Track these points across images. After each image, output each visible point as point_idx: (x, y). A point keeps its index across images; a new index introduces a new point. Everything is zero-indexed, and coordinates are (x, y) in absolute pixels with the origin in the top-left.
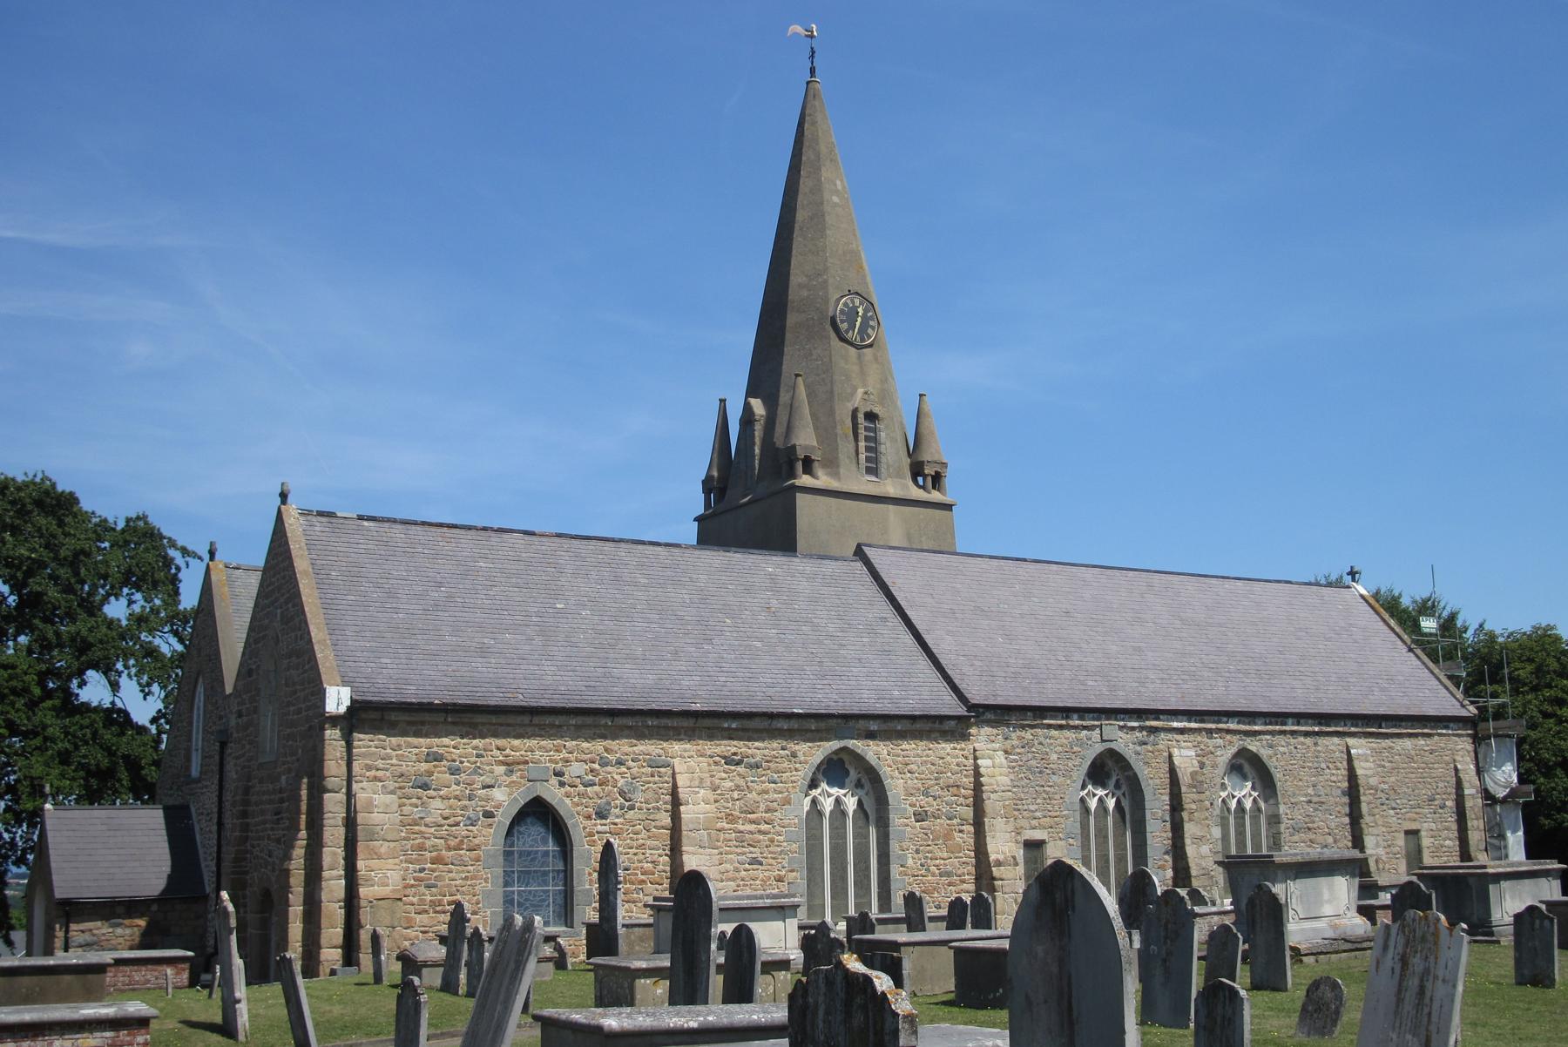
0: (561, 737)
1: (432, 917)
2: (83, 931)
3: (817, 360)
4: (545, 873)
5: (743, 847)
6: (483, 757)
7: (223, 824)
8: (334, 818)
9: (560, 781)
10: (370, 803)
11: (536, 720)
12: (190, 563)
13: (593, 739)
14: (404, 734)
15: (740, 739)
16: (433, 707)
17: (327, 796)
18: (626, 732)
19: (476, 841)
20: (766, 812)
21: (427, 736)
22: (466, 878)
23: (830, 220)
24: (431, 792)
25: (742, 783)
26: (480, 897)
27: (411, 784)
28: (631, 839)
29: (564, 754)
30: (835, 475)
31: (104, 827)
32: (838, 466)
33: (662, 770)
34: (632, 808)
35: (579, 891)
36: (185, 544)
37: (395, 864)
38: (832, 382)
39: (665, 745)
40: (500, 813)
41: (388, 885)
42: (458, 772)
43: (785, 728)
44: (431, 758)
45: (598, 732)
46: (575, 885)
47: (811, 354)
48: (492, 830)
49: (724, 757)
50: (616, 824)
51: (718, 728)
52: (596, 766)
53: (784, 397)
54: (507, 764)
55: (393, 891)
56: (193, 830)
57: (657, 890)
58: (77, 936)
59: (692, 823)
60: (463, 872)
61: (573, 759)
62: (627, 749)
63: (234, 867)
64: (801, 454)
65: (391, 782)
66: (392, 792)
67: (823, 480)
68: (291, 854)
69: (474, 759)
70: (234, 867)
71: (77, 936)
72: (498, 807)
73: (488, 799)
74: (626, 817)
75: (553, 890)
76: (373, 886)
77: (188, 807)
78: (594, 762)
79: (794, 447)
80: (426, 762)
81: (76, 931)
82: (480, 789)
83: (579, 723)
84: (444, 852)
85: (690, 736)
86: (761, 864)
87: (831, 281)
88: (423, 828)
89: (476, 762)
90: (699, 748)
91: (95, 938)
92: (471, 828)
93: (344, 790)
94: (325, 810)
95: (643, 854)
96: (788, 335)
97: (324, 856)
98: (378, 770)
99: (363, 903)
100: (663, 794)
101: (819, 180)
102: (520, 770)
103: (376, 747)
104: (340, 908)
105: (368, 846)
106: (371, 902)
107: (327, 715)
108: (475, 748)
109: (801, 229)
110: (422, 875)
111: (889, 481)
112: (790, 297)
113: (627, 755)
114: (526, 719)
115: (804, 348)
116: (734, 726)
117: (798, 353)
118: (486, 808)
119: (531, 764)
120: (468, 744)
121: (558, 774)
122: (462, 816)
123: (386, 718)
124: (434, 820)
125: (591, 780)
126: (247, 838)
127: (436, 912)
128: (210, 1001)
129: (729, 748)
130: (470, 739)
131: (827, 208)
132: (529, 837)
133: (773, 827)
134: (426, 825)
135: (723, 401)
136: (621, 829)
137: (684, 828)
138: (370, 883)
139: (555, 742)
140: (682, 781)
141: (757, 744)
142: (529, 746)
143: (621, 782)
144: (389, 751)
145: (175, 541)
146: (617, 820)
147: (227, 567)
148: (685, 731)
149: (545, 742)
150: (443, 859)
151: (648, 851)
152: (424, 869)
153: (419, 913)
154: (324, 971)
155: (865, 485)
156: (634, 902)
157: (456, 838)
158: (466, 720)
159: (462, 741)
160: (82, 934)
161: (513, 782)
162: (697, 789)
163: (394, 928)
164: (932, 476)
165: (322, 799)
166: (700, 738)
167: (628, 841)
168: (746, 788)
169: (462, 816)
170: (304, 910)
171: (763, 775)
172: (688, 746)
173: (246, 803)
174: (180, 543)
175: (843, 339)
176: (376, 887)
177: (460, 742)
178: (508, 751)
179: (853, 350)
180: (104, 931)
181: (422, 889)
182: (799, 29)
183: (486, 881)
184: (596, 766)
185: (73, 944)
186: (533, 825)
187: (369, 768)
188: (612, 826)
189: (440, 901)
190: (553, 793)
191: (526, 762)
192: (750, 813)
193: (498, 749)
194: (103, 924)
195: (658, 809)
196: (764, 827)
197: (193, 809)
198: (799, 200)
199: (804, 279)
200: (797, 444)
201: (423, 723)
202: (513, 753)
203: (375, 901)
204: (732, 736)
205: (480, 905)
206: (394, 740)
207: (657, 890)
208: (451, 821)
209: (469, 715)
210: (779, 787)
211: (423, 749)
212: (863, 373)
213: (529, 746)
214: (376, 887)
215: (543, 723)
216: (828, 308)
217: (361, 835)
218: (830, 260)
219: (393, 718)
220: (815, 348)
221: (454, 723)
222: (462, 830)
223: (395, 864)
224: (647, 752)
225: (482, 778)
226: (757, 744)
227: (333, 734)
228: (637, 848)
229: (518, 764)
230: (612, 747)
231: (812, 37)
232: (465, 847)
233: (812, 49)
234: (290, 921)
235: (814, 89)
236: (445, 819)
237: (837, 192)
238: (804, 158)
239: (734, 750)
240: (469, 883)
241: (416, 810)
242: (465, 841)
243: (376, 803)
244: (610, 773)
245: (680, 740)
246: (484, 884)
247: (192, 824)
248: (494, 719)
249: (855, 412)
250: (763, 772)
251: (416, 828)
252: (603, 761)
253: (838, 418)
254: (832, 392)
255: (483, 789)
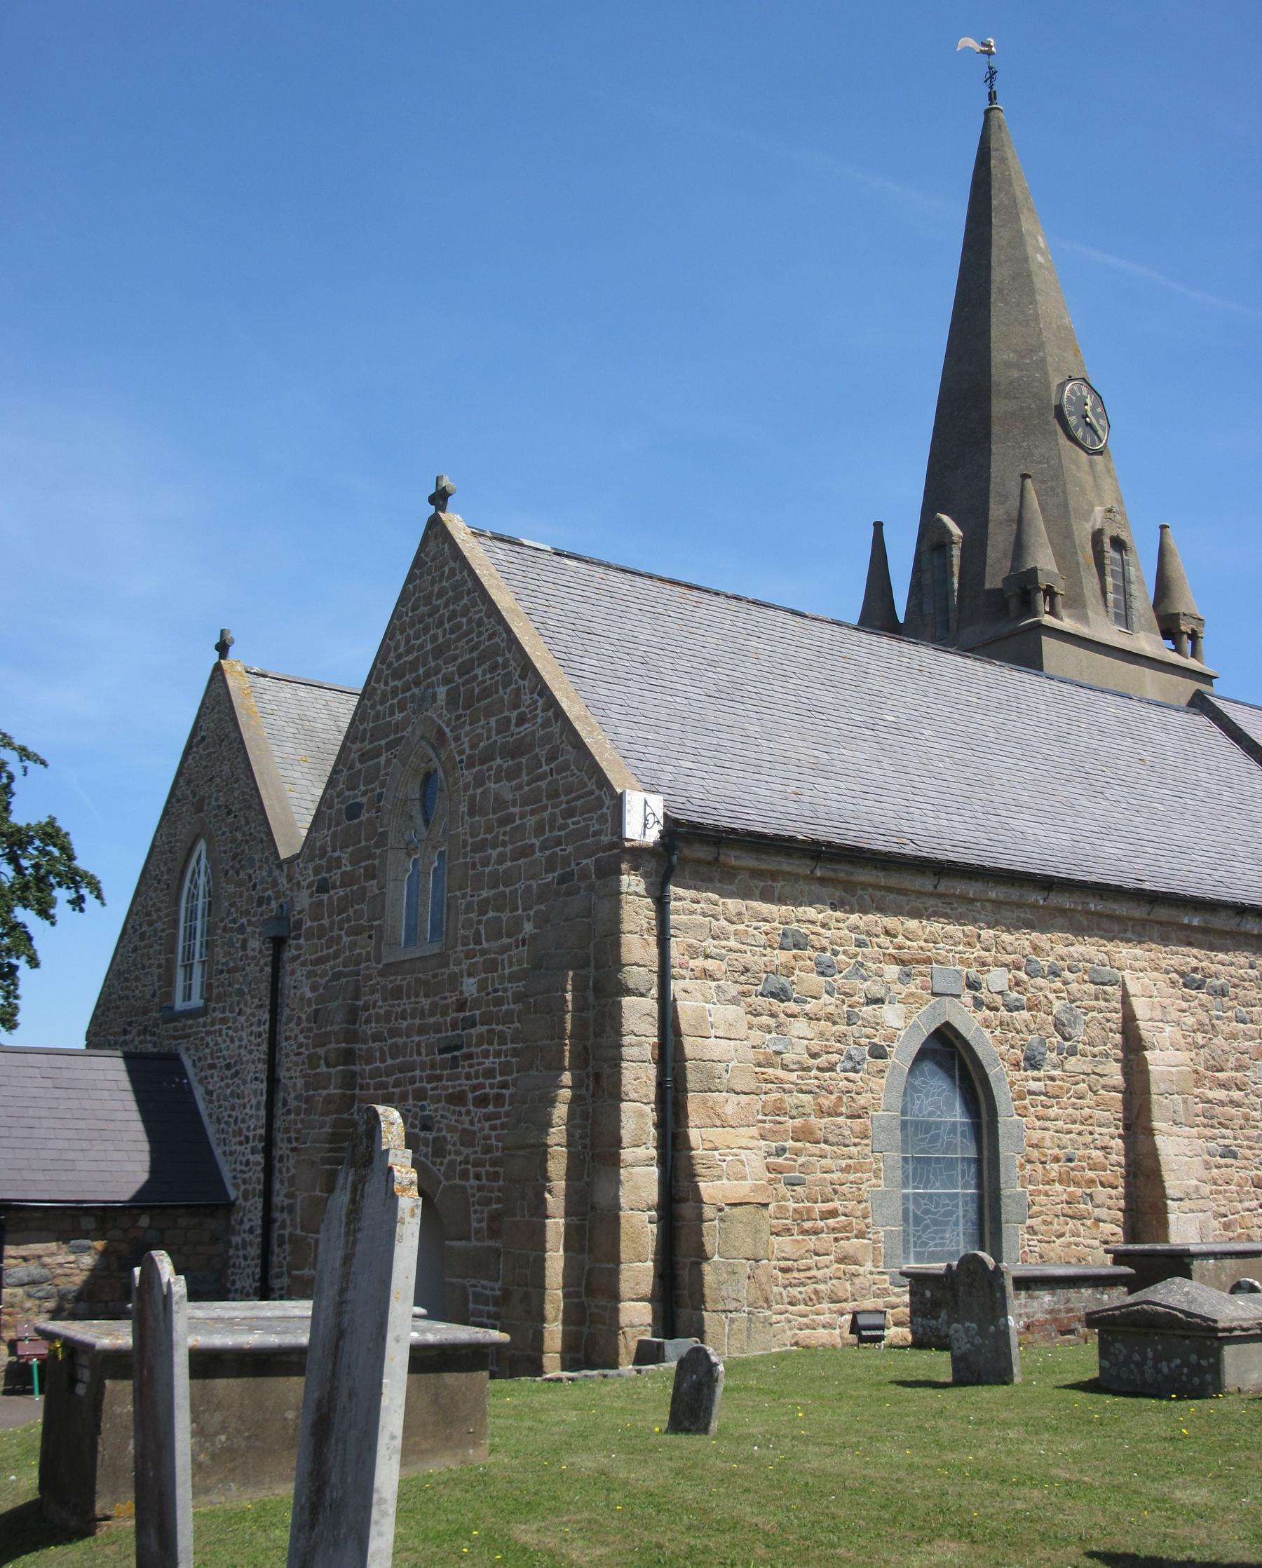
0: (975, 921)
1: (798, 1241)
2: (25, 1259)
3: (1040, 462)
4: (951, 1163)
5: (1212, 1127)
6: (866, 945)
7: (279, 1080)
8: (639, 1044)
9: (975, 998)
10: (701, 1019)
11: (945, 886)
12: (28, 770)
13: (1018, 928)
14: (746, 895)
15: (1201, 947)
16: (795, 845)
17: (627, 1001)
18: (1059, 920)
19: (862, 1100)
20: (1237, 1071)
21: (781, 900)
22: (847, 1169)
23: (1038, 282)
24: (791, 1004)
25: (1204, 1017)
26: (869, 1204)
27: (759, 988)
28: (1074, 1106)
29: (978, 952)
30: (1083, 619)
31: (49, 1083)
32: (1084, 606)
33: (1107, 988)
34: (1072, 1052)
35: (1009, 1197)
36: (24, 744)
37: (752, 1138)
38: (1064, 492)
39: (1110, 947)
40: (894, 1050)
41: (744, 1178)
42: (830, 971)
43: (1256, 932)
44: (790, 941)
45: (1022, 915)
46: (1002, 1186)
47: (1031, 454)
48: (883, 1081)
49: (1182, 974)
50: (1052, 1079)
51: (1173, 924)
52: (1022, 975)
53: (997, 511)
54: (901, 962)
55: (755, 1189)
56: (191, 1093)
57: (1111, 1198)
58: (17, 1266)
59: (1164, 1081)
60: (842, 1157)
61: (990, 960)
62: (1061, 949)
63: (331, 1150)
64: (1043, 582)
65: (730, 983)
66: (734, 1001)
67: (1067, 623)
68: (550, 1115)
69: (853, 949)
70: (331, 1150)
71: (17, 1266)
72: (890, 1039)
73: (876, 1025)
74: (1067, 1067)
75: (964, 1195)
76: (719, 1178)
77: (176, 1058)
78: (1019, 969)
79: (1034, 571)
80: (781, 948)
81: (13, 1257)
82: (863, 1005)
83: (1002, 897)
84: (812, 1118)
85: (1140, 935)
86: (1235, 1157)
87: (1049, 359)
88: (781, 1073)
89: (856, 955)
90: (1152, 955)
91: (45, 1272)
92: (851, 1075)
93: (654, 992)
94: (625, 1029)
95: (1091, 1133)
96: (996, 429)
97: (623, 1117)
98: (707, 957)
99: (708, 1212)
100: (1111, 1030)
101: (1019, 231)
102: (921, 974)
103: (704, 915)
104: (650, 1222)
105: (704, 1102)
106: (721, 1210)
107: (627, 844)
108: (854, 929)
109: (1000, 291)
110: (780, 1160)
111: (1141, 635)
112: (993, 379)
113: (1063, 959)
114: (925, 883)
115: (1021, 447)
116: (1196, 922)
117: (1012, 452)
118: (876, 1040)
119: (934, 965)
120: (844, 921)
121: (973, 985)
122: (840, 1052)
123: (722, 858)
124: (797, 1058)
125: (1017, 1000)
126: (353, 1097)
127: (804, 1232)
128: (689, 1442)
129: (1188, 959)
130: (845, 912)
131: (1033, 267)
132: (927, 1096)
133: (1247, 1095)
134: (785, 1067)
135: (878, 526)
136: (1061, 1087)
137: (1154, 1089)
138: (715, 1172)
139: (965, 928)
140: (1141, 1008)
141: (1221, 956)
142: (931, 932)
143: (1057, 1006)
144: (723, 923)
145: (10, 738)
146: (1054, 1073)
147: (247, 672)
148: (1133, 926)
149: (951, 927)
150: (812, 1133)
151: (1097, 1129)
152: (784, 1150)
153: (778, 1235)
154: (626, 1346)
155: (1110, 634)
156: (1081, 1218)
157: (831, 1093)
158: (842, 875)
159: (835, 913)
160: (24, 1264)
161: (912, 994)
162: (1160, 1024)
163: (757, 1261)
164: (1188, 635)
165: (619, 1006)
166: (1152, 940)
167: (1070, 1110)
168: (1210, 1028)
169: (840, 1052)
170: (567, 1226)
171: (1230, 1008)
172: (1138, 951)
173: (351, 1036)
174: (17, 742)
175: (1072, 439)
176: (725, 1181)
177: (832, 916)
178: (900, 939)
179: (1083, 455)
180: (61, 1259)
181: (782, 1188)
182: (970, 43)
183: (876, 1173)
184: (1022, 975)
185: (8, 1281)
186: (933, 1076)
187: (694, 953)
188: (1048, 1082)
189: (809, 1210)
190: (969, 1022)
191: (928, 961)
192: (1218, 1071)
193: (887, 933)
194: (59, 1248)
195: (1107, 1056)
196: (1237, 1095)
197: (188, 1063)
198: (993, 254)
199: (1011, 355)
200: (1039, 566)
201: (774, 875)
202: (909, 943)
203: (727, 1209)
204: (1192, 940)
205: (869, 1220)
206: (733, 905)
207: (1111, 1198)
208: (822, 1061)
209: (847, 867)
210: (1249, 1029)
211: (776, 924)
212: (1097, 487)
213: (931, 932)
214: (725, 1181)
215: (952, 891)
216: (1050, 395)
217: (693, 1079)
218: (1045, 334)
219: (733, 862)
220: (1036, 447)
221: (822, 881)
222: (838, 1079)
223: (752, 1138)
224: (1087, 957)
225: (865, 985)
226: (1221, 956)
227: (632, 882)
228: (1082, 1123)
229: (918, 962)
230: (1042, 944)
231: (990, 53)
232: (843, 1110)
233: (990, 68)
234: (548, 1246)
235: (998, 118)
236: (814, 1056)
237: (1039, 249)
238: (994, 202)
239: (1194, 963)
240: (851, 1177)
241: (768, 1036)
242: (845, 1099)
243: (711, 1019)
244: (1041, 989)
245: (1128, 941)
246: (874, 1181)
247: (189, 1084)
248: (881, 878)
249: (1097, 536)
250: (1230, 1004)
251: (770, 1071)
252: (1033, 966)
253: (1077, 542)
254: (1066, 505)
255: (867, 1004)
